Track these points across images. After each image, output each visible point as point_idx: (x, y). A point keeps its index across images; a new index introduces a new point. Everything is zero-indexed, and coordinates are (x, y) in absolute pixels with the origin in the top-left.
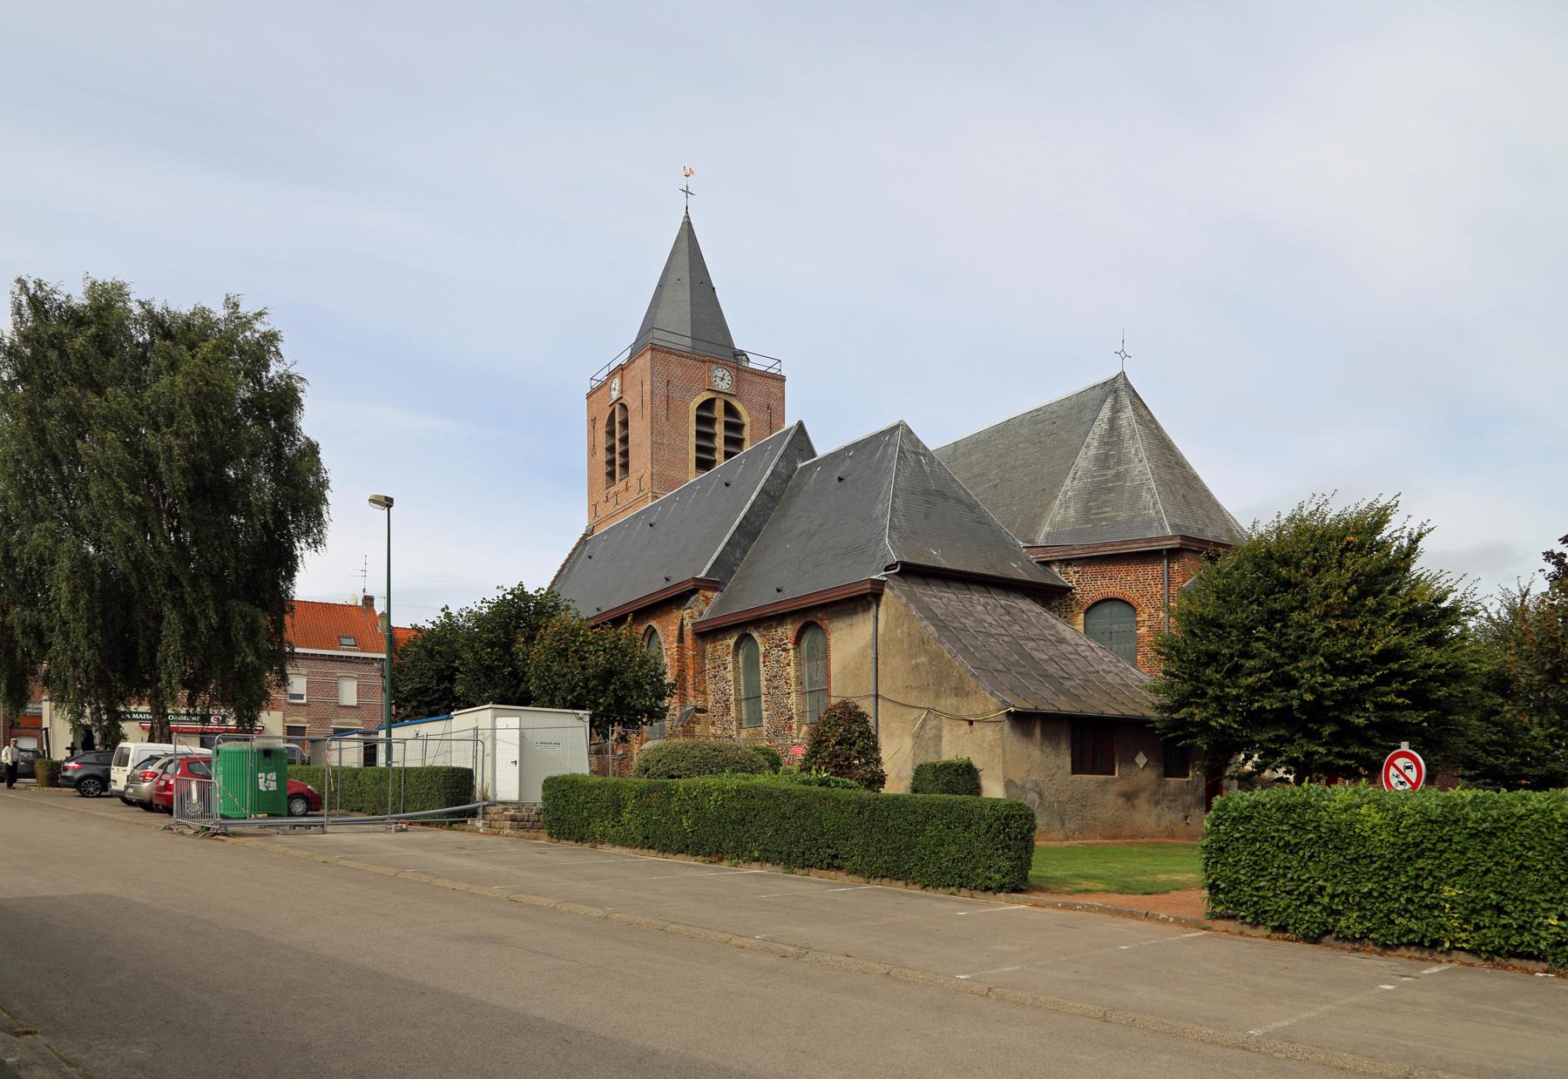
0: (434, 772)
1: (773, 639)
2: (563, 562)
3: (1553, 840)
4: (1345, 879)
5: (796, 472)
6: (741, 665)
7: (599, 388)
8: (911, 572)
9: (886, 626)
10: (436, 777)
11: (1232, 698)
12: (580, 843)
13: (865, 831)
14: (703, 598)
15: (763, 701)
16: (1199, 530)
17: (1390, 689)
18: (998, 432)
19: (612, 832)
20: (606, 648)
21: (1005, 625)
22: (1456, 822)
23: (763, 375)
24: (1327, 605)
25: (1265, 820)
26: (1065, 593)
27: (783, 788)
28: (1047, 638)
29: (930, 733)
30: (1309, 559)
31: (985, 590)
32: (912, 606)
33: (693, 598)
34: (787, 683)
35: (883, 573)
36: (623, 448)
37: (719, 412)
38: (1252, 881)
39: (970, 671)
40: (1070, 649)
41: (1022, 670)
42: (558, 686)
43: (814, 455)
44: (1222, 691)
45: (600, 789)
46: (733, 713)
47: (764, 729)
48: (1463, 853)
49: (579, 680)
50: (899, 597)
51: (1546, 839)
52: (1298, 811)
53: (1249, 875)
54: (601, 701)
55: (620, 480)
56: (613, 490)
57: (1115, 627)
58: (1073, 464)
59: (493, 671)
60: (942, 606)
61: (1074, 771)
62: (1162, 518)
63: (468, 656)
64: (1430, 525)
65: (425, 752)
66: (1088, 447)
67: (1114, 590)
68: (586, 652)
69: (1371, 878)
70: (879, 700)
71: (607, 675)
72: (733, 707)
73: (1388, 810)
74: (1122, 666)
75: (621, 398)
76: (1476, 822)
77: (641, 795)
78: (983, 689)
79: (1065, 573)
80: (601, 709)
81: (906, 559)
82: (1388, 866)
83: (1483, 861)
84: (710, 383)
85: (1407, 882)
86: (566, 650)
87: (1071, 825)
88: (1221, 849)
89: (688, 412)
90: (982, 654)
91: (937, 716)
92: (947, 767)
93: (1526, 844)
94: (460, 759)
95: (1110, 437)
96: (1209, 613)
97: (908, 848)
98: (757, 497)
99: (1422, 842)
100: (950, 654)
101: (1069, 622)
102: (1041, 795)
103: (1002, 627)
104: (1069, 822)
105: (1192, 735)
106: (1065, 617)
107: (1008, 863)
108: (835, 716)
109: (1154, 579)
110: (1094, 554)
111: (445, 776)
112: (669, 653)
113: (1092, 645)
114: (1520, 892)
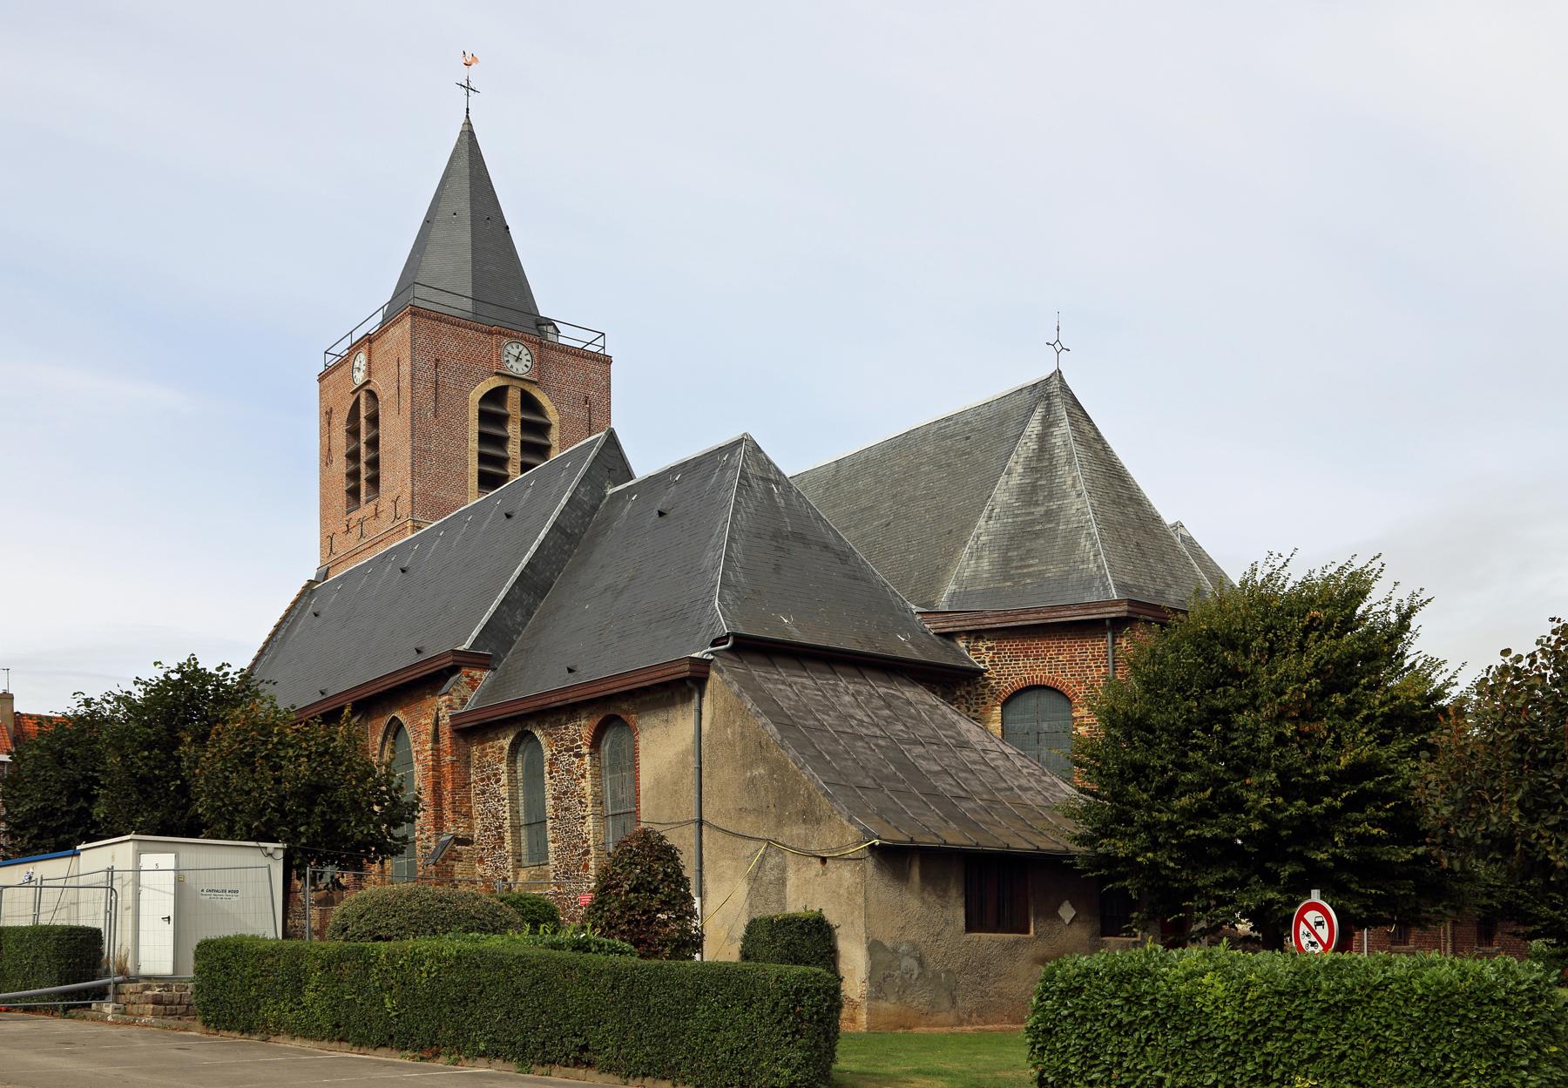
0: (40, 934)
1: (562, 739)
2: (276, 620)
3: (1411, 1015)
4: (1187, 1069)
5: (605, 501)
6: (520, 775)
7: (337, 367)
8: (747, 648)
9: (712, 723)
10: (45, 941)
11: (1165, 826)
12: (246, 1035)
13: (621, 1012)
14: (467, 680)
15: (548, 828)
16: (1157, 592)
17: (1364, 816)
18: (894, 448)
19: (290, 1017)
20: (311, 753)
21: (882, 723)
22: (1306, 993)
24: (1280, 704)
25: (1096, 993)
26: (974, 678)
27: (516, 954)
28: (941, 740)
29: (770, 875)
30: (1260, 640)
31: (856, 673)
32: (746, 697)
33: (452, 679)
34: (581, 803)
35: (710, 649)
36: (372, 455)
37: (513, 406)
38: (1084, 1072)
39: (823, 788)
40: (974, 756)
41: (901, 786)
42: (240, 807)
43: (630, 476)
44: (1150, 816)
45: (273, 956)
46: (508, 846)
47: (551, 868)
48: (1315, 1033)
49: (270, 799)
50: (728, 684)
51: (1404, 1014)
52: (1134, 980)
53: (1079, 1064)
54: (302, 829)
55: (367, 502)
56: (356, 515)
57: (1045, 726)
58: (989, 497)
59: (151, 784)
60: (791, 695)
61: (969, 928)
62: (1105, 575)
63: (113, 760)
64: (1424, 596)
65: (37, 904)
66: (1009, 474)
67: (1041, 673)
68: (283, 758)
69: (1215, 1067)
70: (704, 828)
71: (313, 792)
72: (508, 836)
73: (1234, 978)
74: (1049, 780)
75: (368, 382)
76: (1328, 994)
77: (329, 966)
78: (839, 813)
79: (974, 650)
80: (304, 840)
81: (742, 630)
82: (1232, 1051)
83: (1337, 1043)
84: (500, 364)
85: (1254, 1070)
86: (252, 755)
87: (966, 1004)
88: (1048, 1031)
89: (467, 405)
90: (844, 763)
91: (779, 851)
92: (789, 922)
93: (1382, 1020)
94: (89, 915)
95: (1039, 460)
96: (1137, 709)
97: (674, 1035)
98: (547, 536)
99: (1268, 1019)
100: (796, 764)
101: (980, 719)
102: (921, 961)
103: (878, 726)
104: (964, 1000)
105: (1123, 877)
106: (976, 711)
107: (799, 1054)
108: (631, 851)
109: (1094, 659)
110: (1014, 624)
111: (58, 940)
112: (421, 758)
113: (1008, 750)
114: (1379, 1082)
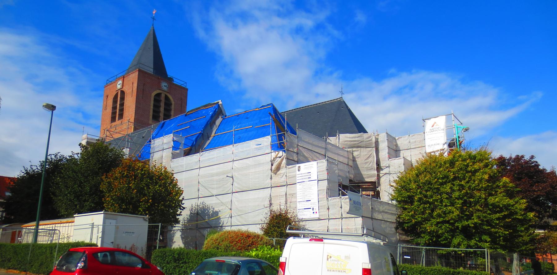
23: (180, 87)
55: (118, 120)
56: (114, 124)
